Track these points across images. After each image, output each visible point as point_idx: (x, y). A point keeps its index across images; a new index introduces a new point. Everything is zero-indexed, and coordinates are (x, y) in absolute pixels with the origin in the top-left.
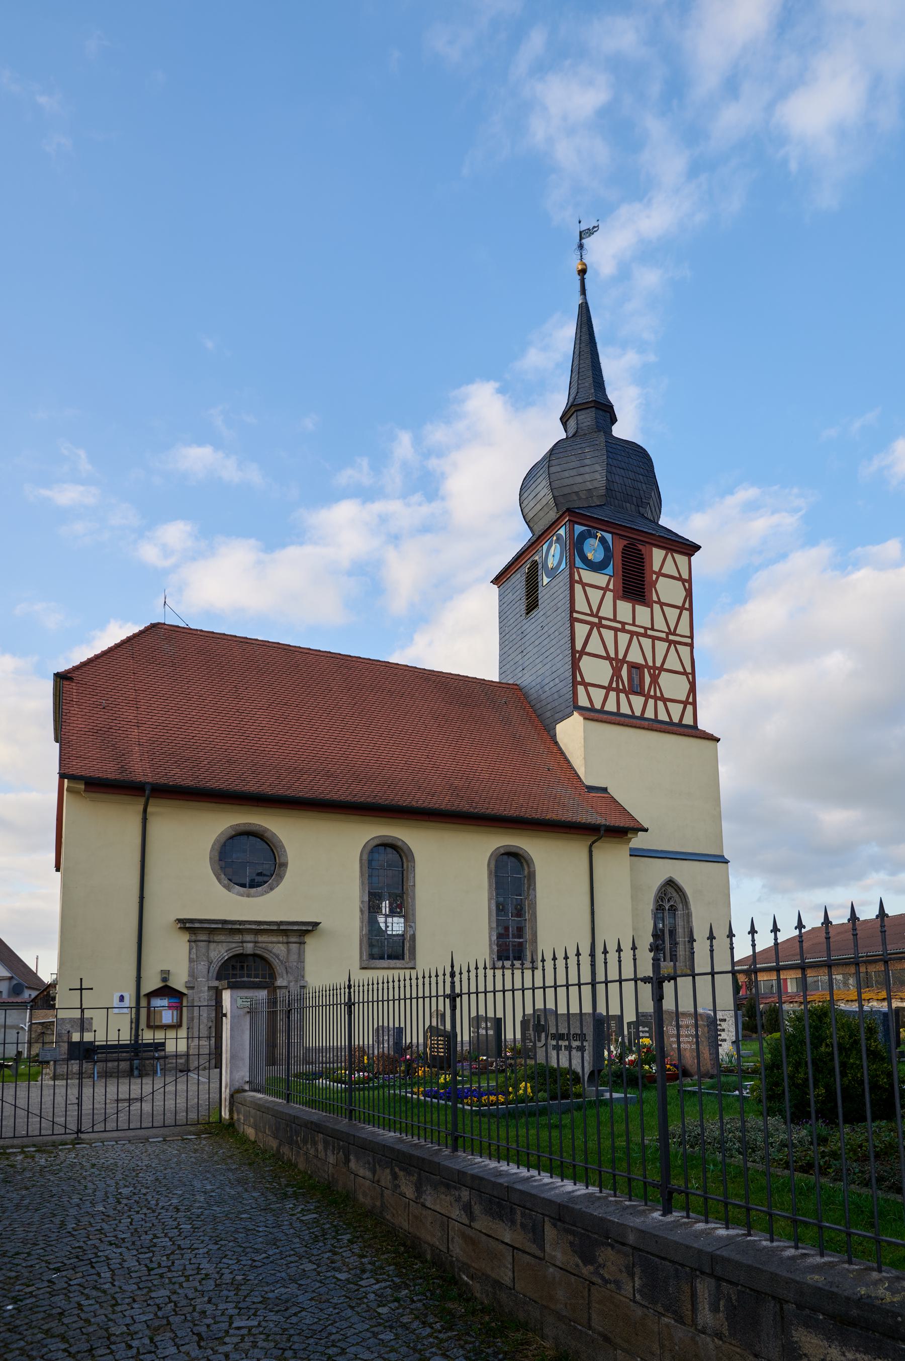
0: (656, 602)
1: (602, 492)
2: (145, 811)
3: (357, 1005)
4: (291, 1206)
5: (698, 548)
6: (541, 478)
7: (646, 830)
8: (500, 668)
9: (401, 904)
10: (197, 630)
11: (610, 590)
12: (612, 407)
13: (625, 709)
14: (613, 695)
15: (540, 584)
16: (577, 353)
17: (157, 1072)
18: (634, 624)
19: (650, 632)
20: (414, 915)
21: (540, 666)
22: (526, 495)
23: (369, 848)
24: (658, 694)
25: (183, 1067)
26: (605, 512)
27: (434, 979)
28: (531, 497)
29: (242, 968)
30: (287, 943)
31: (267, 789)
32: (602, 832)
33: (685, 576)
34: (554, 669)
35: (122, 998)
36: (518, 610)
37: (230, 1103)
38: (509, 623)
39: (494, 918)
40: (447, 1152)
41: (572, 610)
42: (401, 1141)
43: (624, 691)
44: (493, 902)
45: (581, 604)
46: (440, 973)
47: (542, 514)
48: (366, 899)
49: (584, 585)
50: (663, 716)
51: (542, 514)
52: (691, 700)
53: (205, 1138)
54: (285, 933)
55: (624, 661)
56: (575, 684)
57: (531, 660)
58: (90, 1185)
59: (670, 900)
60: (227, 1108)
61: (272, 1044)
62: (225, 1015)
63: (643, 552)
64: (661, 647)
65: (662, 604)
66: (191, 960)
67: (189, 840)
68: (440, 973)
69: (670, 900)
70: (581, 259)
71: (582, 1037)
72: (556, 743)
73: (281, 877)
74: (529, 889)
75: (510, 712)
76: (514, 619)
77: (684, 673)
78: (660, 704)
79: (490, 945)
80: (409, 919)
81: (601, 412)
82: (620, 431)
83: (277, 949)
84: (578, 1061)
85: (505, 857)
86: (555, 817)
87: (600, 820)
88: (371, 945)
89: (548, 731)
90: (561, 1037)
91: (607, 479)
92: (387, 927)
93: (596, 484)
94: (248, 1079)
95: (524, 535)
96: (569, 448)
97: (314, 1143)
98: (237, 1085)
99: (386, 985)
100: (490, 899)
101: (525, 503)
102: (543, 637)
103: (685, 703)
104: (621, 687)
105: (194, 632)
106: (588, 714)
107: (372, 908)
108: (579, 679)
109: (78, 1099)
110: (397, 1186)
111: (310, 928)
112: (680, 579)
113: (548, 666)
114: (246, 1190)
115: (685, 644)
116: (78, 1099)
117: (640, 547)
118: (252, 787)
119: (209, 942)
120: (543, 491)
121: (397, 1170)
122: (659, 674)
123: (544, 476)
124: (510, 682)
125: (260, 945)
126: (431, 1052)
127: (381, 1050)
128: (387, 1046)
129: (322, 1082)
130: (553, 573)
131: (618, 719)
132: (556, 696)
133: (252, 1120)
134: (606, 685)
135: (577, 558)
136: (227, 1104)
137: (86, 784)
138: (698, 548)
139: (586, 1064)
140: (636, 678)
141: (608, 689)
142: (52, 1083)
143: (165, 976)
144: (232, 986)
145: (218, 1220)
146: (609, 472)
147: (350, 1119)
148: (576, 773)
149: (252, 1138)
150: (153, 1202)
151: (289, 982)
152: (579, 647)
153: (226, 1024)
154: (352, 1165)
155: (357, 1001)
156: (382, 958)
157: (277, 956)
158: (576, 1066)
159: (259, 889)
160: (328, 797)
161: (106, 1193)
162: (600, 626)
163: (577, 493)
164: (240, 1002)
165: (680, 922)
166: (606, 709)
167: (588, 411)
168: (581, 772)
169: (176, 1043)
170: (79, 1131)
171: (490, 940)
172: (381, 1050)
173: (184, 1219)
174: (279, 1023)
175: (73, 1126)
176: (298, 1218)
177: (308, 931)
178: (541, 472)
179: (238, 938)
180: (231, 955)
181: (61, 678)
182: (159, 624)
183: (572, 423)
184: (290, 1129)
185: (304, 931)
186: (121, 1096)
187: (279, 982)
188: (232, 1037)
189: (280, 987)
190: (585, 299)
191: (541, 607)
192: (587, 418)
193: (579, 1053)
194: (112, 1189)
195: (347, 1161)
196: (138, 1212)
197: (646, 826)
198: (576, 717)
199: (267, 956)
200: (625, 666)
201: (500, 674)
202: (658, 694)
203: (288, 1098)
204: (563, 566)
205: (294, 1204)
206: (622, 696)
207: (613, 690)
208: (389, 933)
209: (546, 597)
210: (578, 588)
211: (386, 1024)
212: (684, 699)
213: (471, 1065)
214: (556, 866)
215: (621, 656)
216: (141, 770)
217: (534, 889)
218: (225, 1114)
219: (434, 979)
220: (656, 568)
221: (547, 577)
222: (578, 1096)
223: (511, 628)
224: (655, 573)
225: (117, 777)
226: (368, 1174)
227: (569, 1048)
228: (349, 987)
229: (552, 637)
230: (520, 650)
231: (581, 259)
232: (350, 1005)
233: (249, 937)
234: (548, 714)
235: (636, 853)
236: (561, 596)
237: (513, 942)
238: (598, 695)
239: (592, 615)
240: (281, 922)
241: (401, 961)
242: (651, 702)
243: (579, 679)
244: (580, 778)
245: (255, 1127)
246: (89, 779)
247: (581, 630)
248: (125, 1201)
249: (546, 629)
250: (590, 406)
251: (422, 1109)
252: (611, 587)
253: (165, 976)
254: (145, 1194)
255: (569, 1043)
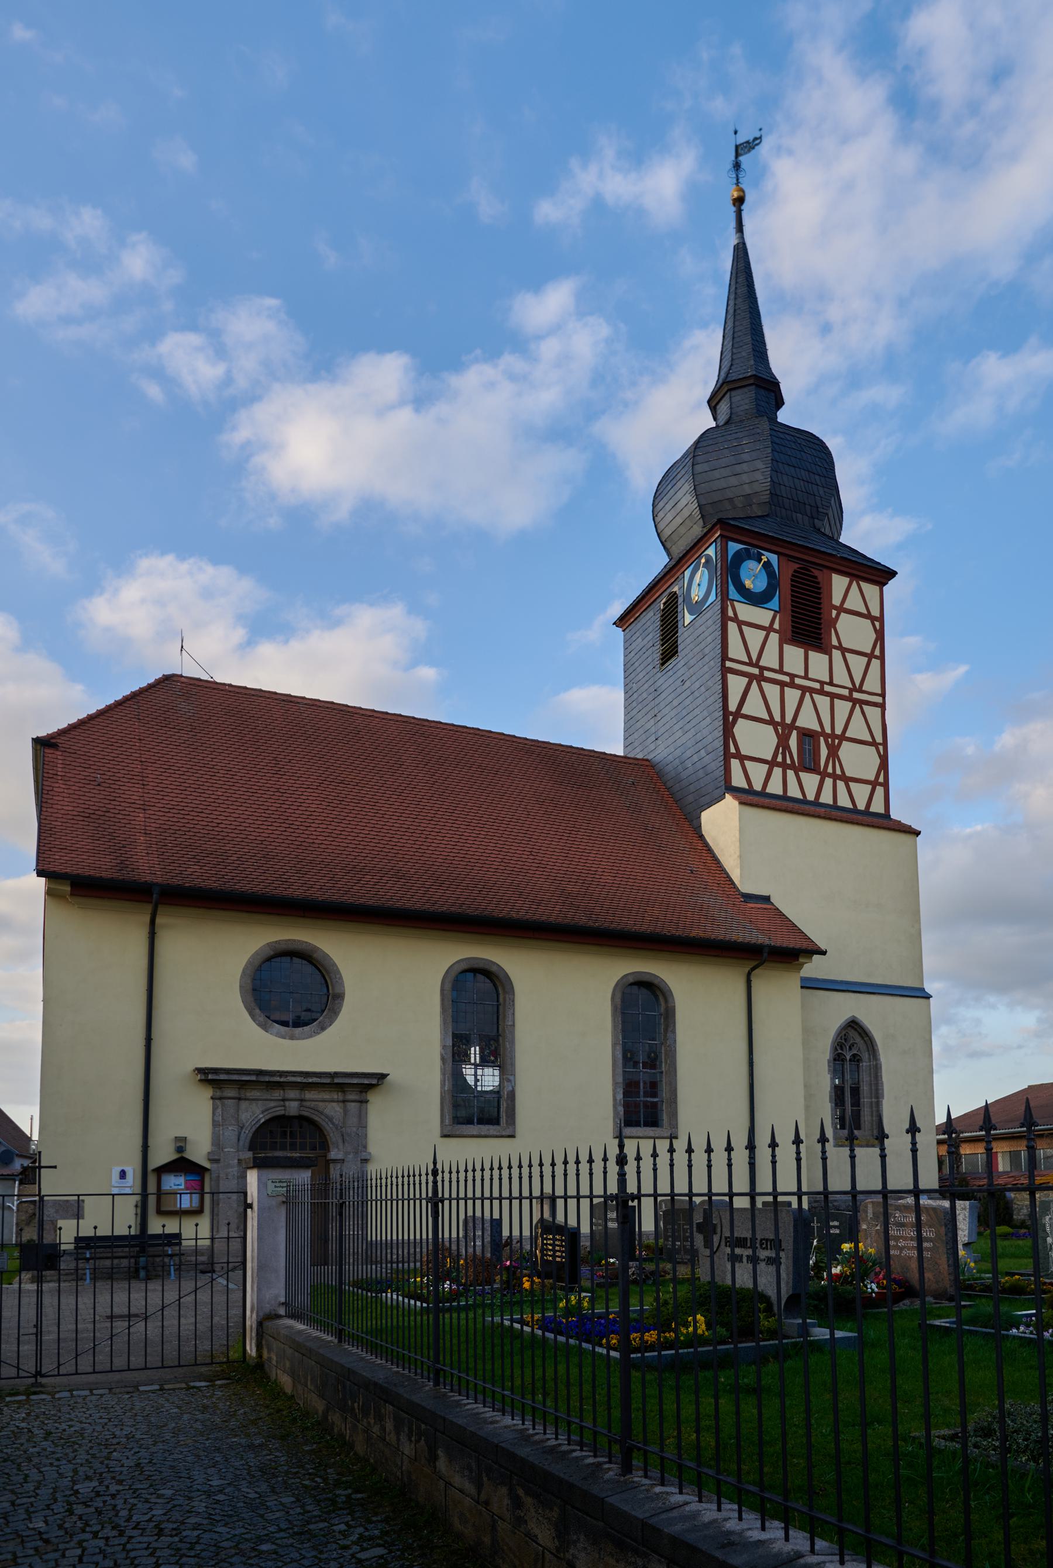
0: (836, 648)
1: (765, 498)
2: (153, 922)
3: (446, 1203)
4: (343, 1527)
5: (893, 574)
6: (683, 481)
7: (824, 953)
8: (625, 739)
9: (497, 1053)
10: (224, 684)
11: (775, 631)
12: (777, 384)
13: (794, 792)
14: (777, 771)
15: (680, 624)
16: (731, 311)
17: (169, 1274)
18: (806, 677)
19: (827, 688)
20: (513, 1065)
21: (680, 733)
22: (661, 504)
23: (453, 974)
24: (838, 772)
25: (206, 1266)
26: (767, 519)
27: (584, 1167)
28: (668, 507)
29: (284, 1134)
30: (344, 1101)
31: (316, 894)
32: (765, 955)
33: (876, 613)
34: (699, 737)
35: (123, 1175)
36: (650, 660)
37: (257, 1334)
38: (637, 679)
39: (620, 1070)
40: (612, 1472)
41: (725, 657)
42: (525, 1438)
43: (792, 767)
44: (619, 1048)
45: (736, 650)
46: (598, 1157)
47: (682, 530)
48: (449, 1042)
49: (740, 624)
50: (844, 801)
51: (682, 530)
52: (881, 780)
53: (221, 1386)
54: (341, 1087)
55: (792, 726)
56: (727, 757)
57: (667, 726)
58: (34, 1475)
59: (853, 1055)
60: (254, 1341)
61: (320, 1238)
62: (250, 1206)
63: (820, 579)
64: (843, 708)
65: (844, 651)
66: (215, 1124)
67: (211, 965)
68: (598, 1157)
69: (853, 1055)
70: (738, 183)
71: (776, 1244)
72: (701, 837)
73: (335, 1013)
74: (666, 1030)
75: (640, 799)
76: (644, 673)
77: (873, 743)
78: (841, 784)
79: (615, 1106)
80: (506, 1070)
81: (762, 392)
82: (784, 416)
83: (330, 1109)
84: (771, 1281)
85: (635, 987)
86: (702, 935)
87: (761, 939)
88: (456, 1106)
89: (691, 821)
90: (741, 1242)
91: (772, 481)
92: (477, 1080)
93: (757, 487)
94: (283, 1300)
95: (660, 560)
96: (721, 440)
97: (380, 1418)
98: (267, 1308)
99: (496, 1172)
100: (614, 1045)
101: (661, 515)
102: (684, 696)
103: (874, 784)
104: (789, 761)
105: (221, 687)
106: (744, 797)
107: (457, 1055)
108: (733, 750)
109: (36, 1326)
110: (520, 1521)
111: (374, 1082)
112: (868, 616)
113: (690, 735)
114: (273, 1491)
115: (875, 704)
116: (36, 1326)
117: (816, 573)
118: (296, 891)
119: (240, 1099)
120: (685, 500)
121: (521, 1492)
122: (840, 744)
123: (686, 477)
124: (638, 757)
125: (308, 1104)
126: (543, 1255)
127: (470, 1250)
128: (480, 1244)
129: (391, 1296)
130: (697, 609)
131: (784, 804)
132: (701, 773)
133: (288, 1364)
134: (769, 758)
135: (731, 588)
136: (254, 1335)
137: (73, 885)
138: (893, 574)
139: (783, 1285)
140: (808, 750)
141: (772, 764)
142: (34, 1287)
143: (181, 1144)
144: (259, 1164)
145: (222, 1555)
146: (775, 470)
147: (437, 1383)
148: (728, 876)
149: (288, 1390)
150: (124, 1513)
151: (347, 1153)
152: (733, 707)
153: (252, 1216)
154: (442, 1464)
155: (447, 1195)
156: (470, 1122)
157: (331, 1119)
158: (766, 1282)
159: (306, 1028)
160: (398, 905)
161: (55, 1490)
162: (760, 679)
163: (730, 500)
164: (271, 1187)
165: (865, 1078)
166: (768, 790)
167: (746, 390)
168: (735, 875)
169: (195, 1232)
170: (38, 1373)
171: (615, 1099)
172: (470, 1250)
173: (168, 1552)
174: (329, 1215)
175: (29, 1366)
176: (353, 1556)
177: (370, 1087)
178: (683, 472)
179: (277, 1094)
180: (267, 1117)
181: (41, 744)
182: (174, 675)
183: (724, 408)
184: (344, 1386)
185: (364, 1086)
186: (117, 1311)
187: (333, 1154)
188: (260, 1238)
189: (335, 1161)
190: (742, 238)
191: (681, 654)
192: (744, 399)
193: (772, 1269)
194: (66, 1482)
195: (433, 1458)
196: (95, 1535)
197: (823, 948)
198: (729, 802)
199: (316, 1118)
200: (795, 733)
201: (625, 747)
202: (838, 772)
203: (340, 1335)
204: (712, 598)
205: (347, 1524)
206: (790, 773)
207: (779, 765)
208: (479, 1089)
209: (688, 641)
210: (732, 627)
211: (478, 1214)
212: (872, 778)
213: (592, 1271)
214: (703, 1003)
215: (788, 720)
216: (147, 867)
217: (674, 1032)
218: (251, 1349)
219: (584, 1167)
220: (836, 601)
221: (691, 614)
222: (773, 1334)
223: (640, 684)
224: (835, 608)
225: (115, 875)
226: (469, 1487)
227: (754, 1260)
228: (435, 1173)
229: (696, 694)
230: (652, 713)
231: (738, 183)
232: (435, 1201)
233: (292, 1094)
234: (690, 798)
235: (810, 985)
236: (709, 639)
237: (645, 1098)
238: (757, 773)
239: (750, 664)
240: (336, 1073)
241: (496, 1127)
242: (829, 782)
243: (733, 750)
244: (733, 883)
245: (293, 1374)
246: (78, 879)
247: (736, 684)
248: (79, 1510)
249: (688, 684)
250: (748, 384)
251: (538, 1352)
252: (776, 626)
253: (181, 1144)
254: (113, 1496)
255: (754, 1252)
